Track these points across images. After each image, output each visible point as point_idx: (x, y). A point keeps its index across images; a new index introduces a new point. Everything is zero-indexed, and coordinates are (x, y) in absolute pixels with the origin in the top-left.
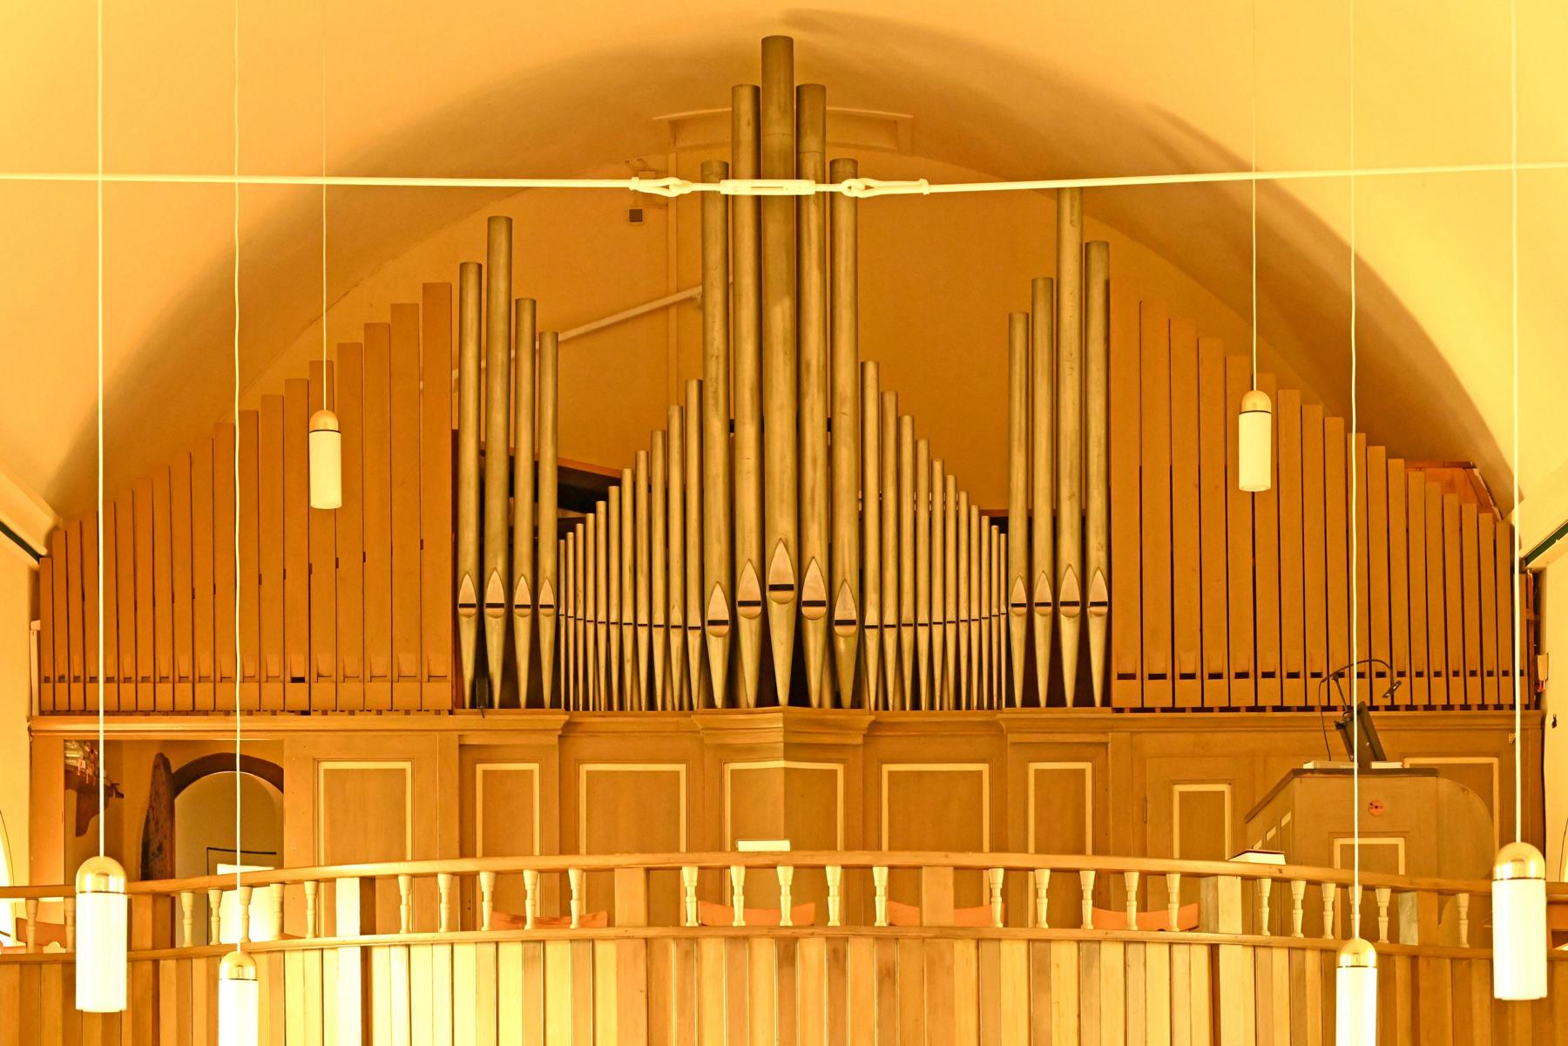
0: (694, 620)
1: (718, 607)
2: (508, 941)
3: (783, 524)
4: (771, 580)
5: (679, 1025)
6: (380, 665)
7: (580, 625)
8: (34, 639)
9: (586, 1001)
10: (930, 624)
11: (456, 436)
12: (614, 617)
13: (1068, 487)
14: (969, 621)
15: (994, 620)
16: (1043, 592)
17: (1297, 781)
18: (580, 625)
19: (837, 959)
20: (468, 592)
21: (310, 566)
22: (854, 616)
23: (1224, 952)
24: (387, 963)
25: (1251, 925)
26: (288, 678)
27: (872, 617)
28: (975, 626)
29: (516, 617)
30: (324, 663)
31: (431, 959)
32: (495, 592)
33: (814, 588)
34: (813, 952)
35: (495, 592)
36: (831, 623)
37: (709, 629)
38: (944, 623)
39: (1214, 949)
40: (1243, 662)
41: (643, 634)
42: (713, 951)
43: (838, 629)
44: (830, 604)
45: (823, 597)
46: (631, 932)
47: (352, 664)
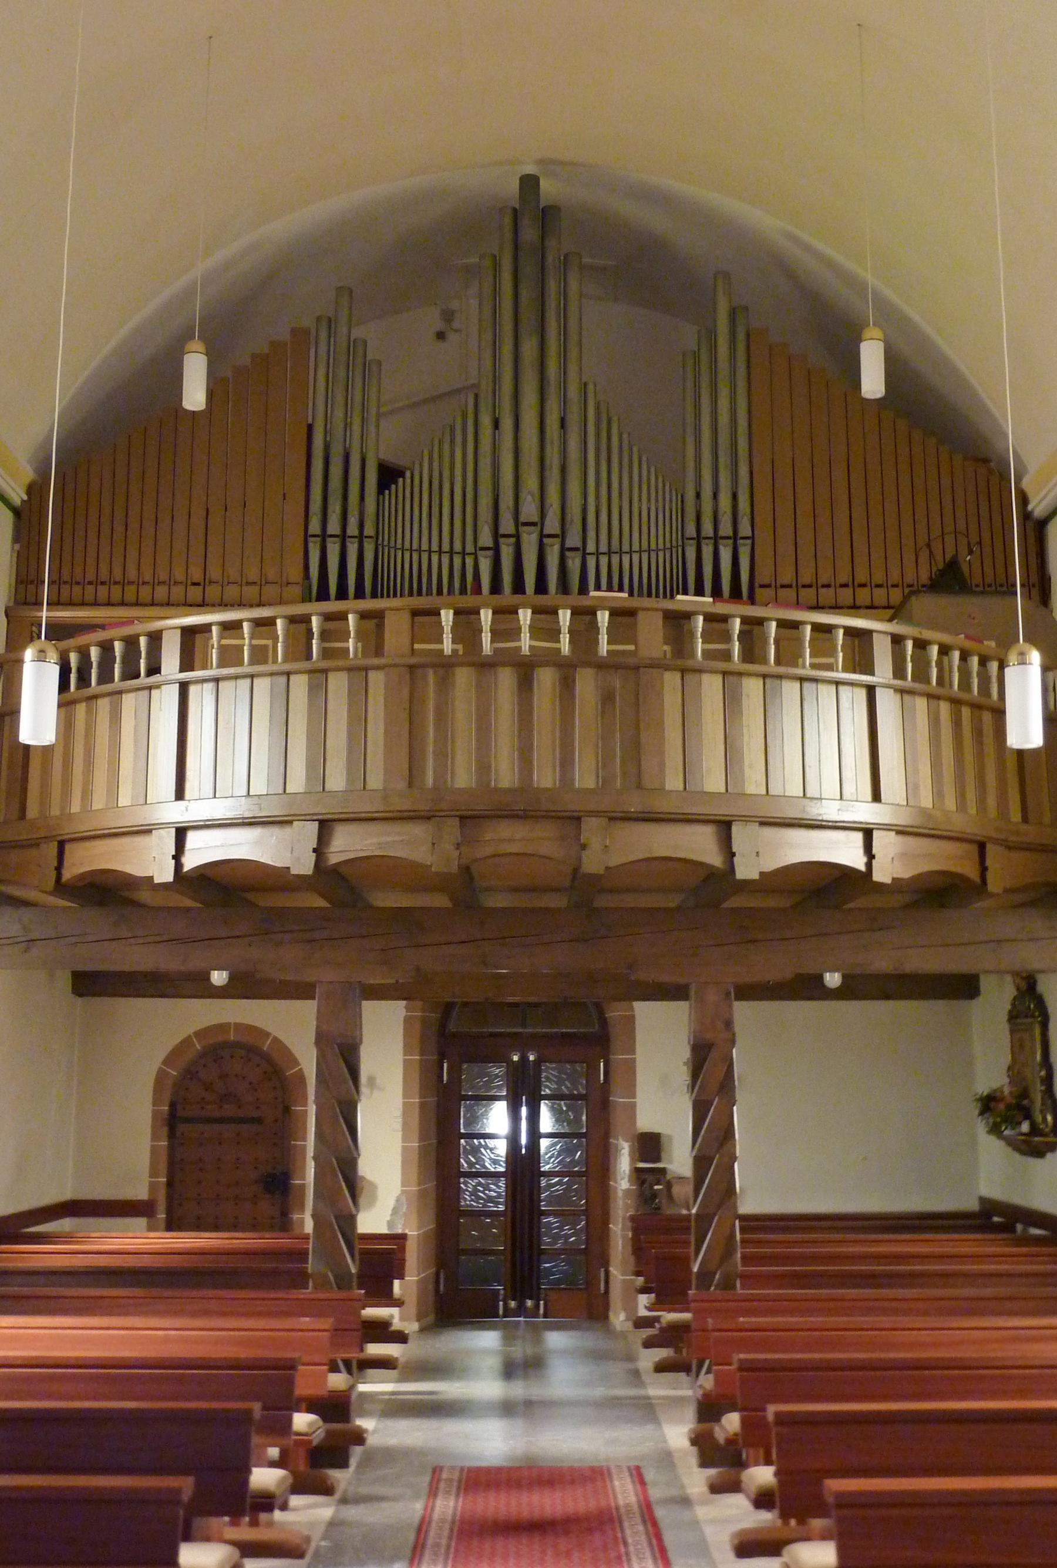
0: (470, 548)
1: (486, 538)
2: (297, 672)
3: (531, 482)
4: (522, 519)
5: (435, 737)
6: (253, 574)
7: (392, 551)
8: (15, 555)
9: (358, 721)
10: (631, 552)
11: (310, 428)
12: (415, 546)
13: (724, 461)
14: (657, 550)
15: (674, 550)
16: (708, 529)
17: (913, 598)
18: (392, 551)
19: (567, 685)
20: (315, 527)
21: (207, 510)
22: (579, 545)
23: (879, 692)
24: (201, 699)
25: (899, 672)
26: (189, 583)
27: (591, 547)
28: (661, 554)
29: (348, 544)
30: (214, 572)
31: (235, 692)
32: (333, 527)
33: (552, 525)
34: (546, 678)
35: (333, 527)
36: (563, 549)
37: (479, 553)
38: (640, 551)
39: (871, 690)
40: (844, 577)
41: (435, 558)
42: (463, 677)
43: (568, 554)
44: (563, 535)
45: (558, 531)
46: (397, 661)
47: (233, 573)
